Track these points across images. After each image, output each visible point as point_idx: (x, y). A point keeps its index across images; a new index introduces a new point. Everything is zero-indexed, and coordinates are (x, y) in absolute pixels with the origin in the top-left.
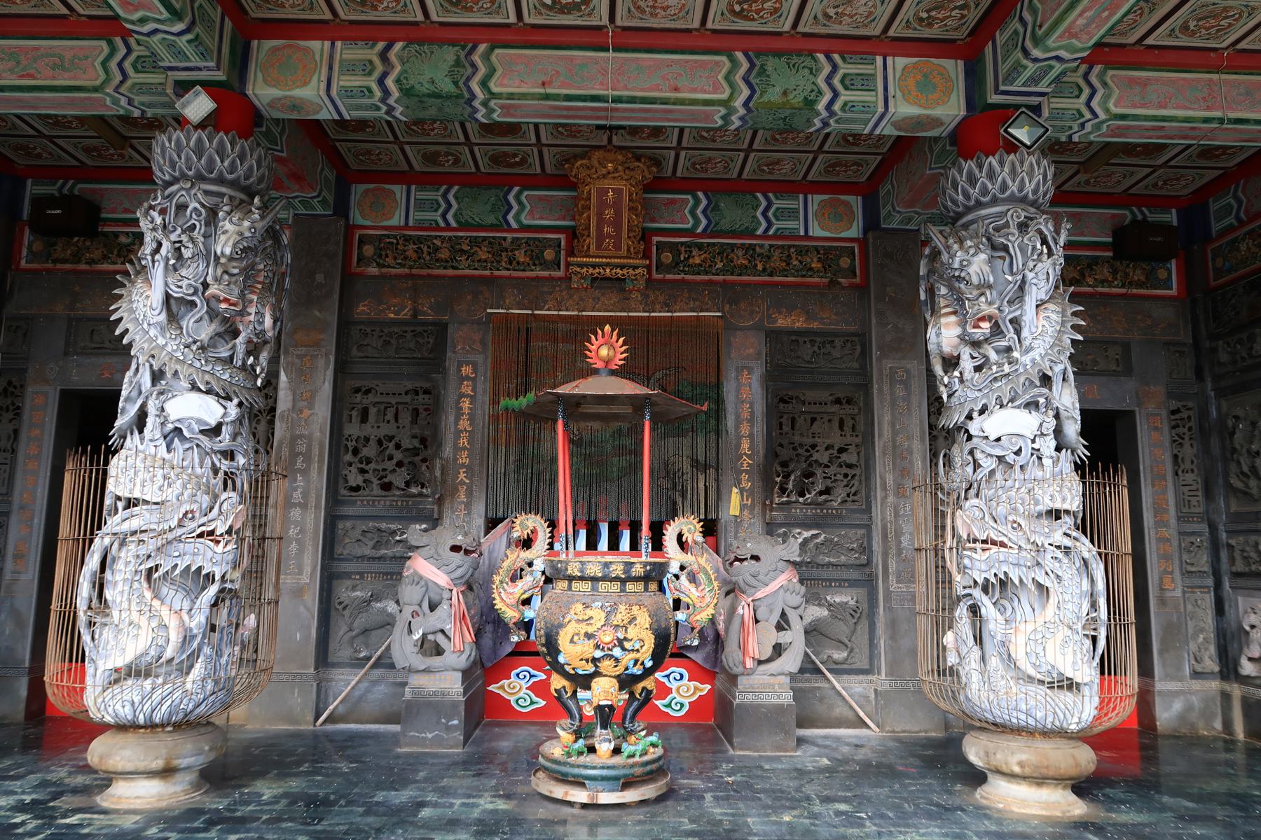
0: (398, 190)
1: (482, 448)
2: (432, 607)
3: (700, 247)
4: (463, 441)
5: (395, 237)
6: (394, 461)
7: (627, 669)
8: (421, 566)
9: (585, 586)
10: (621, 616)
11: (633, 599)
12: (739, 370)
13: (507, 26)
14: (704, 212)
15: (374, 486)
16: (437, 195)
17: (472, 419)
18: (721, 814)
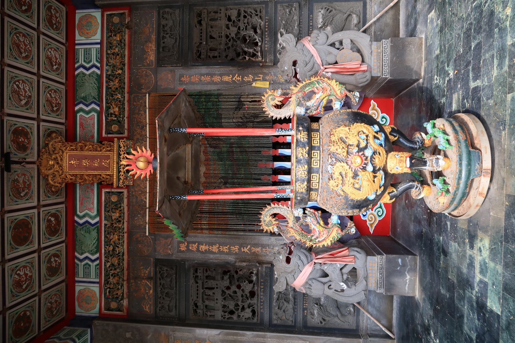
0: (78, 288)
1: (230, 238)
2: (326, 275)
3: (108, 108)
4: (225, 249)
5: (106, 290)
6: (237, 290)
7: (381, 145)
8: (299, 282)
9: (315, 178)
10: (340, 150)
11: (325, 140)
12: (181, 83)
13: (66, 207)
14: (87, 106)
15: (252, 302)
16: (81, 265)
17: (211, 244)
18: (500, 65)
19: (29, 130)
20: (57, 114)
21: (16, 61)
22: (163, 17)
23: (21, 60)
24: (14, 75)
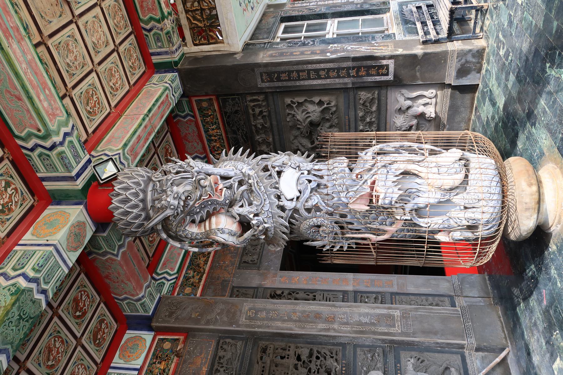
22: (221, 347)
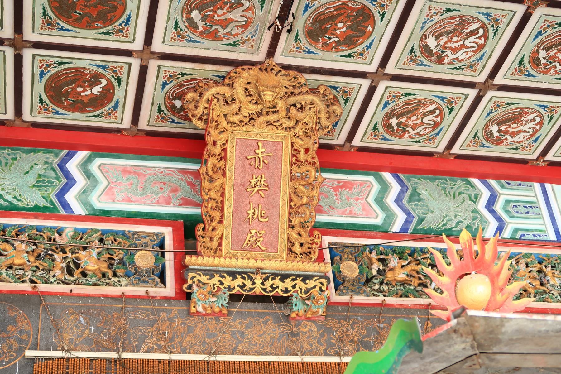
3: (400, 253)
14: (398, 201)
19: (359, 48)
20: (380, 127)
21: (533, 36)
23: (532, 45)
24: (502, 26)
